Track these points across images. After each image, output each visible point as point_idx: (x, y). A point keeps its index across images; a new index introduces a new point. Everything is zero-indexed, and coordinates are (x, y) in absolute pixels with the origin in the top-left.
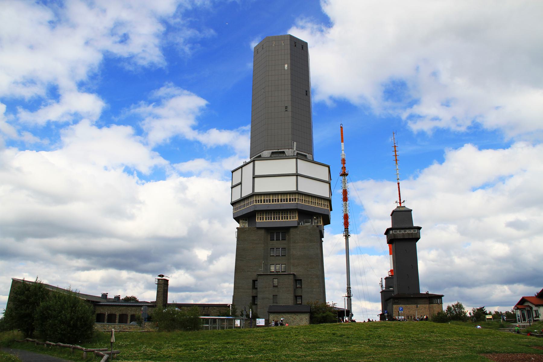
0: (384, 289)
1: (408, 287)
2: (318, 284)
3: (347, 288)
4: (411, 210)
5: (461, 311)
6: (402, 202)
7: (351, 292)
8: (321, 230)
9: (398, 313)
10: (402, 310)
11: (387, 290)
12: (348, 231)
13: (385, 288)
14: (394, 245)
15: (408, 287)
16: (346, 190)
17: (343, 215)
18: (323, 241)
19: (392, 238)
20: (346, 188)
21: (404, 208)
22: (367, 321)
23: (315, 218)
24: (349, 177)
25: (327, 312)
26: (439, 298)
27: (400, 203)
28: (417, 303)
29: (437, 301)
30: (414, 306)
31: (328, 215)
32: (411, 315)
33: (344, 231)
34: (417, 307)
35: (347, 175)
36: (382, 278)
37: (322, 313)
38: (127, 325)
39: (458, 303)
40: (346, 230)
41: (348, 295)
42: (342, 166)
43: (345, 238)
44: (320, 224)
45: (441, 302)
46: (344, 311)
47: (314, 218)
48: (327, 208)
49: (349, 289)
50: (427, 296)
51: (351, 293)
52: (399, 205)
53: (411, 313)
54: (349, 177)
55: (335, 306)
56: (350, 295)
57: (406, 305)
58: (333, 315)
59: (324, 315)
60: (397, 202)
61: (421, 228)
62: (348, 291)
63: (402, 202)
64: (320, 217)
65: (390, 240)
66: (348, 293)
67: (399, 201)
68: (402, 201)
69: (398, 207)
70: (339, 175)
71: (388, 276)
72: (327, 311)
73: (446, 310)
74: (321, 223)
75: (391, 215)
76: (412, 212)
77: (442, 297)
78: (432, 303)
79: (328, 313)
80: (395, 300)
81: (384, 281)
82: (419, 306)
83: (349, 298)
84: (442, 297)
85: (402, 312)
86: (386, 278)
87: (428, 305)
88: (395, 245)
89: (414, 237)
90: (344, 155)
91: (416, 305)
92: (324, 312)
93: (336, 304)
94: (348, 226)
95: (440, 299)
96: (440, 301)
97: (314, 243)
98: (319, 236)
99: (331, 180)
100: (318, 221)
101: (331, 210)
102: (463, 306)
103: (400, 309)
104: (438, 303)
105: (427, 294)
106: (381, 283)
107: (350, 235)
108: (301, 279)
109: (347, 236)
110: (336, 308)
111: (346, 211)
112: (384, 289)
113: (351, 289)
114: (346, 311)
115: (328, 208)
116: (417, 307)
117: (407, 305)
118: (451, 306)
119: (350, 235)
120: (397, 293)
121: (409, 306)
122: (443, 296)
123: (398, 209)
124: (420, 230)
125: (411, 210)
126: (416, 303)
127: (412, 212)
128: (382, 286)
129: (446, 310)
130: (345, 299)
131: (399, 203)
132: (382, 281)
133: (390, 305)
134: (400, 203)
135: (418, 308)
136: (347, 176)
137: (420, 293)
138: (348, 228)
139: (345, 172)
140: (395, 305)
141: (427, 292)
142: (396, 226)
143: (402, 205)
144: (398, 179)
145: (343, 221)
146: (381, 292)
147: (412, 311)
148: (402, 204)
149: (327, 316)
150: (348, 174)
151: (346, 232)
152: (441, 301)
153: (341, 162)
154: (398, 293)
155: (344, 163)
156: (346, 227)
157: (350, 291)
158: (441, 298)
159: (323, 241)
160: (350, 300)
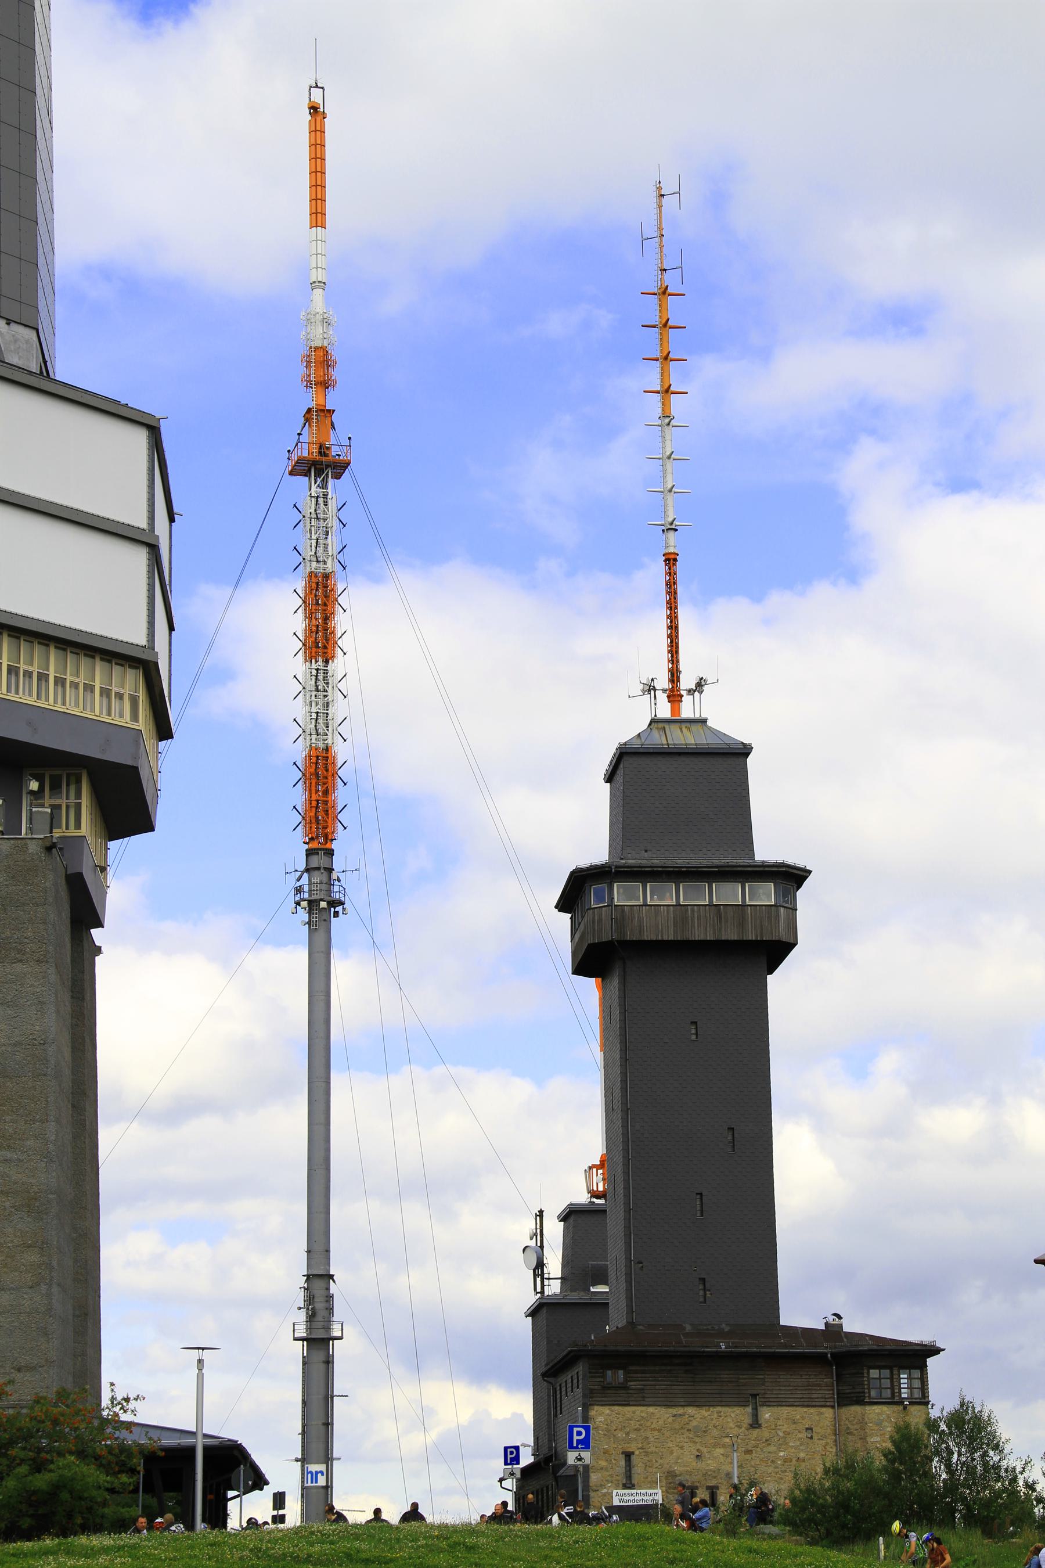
0: (554, 1288)
1: (703, 1280)
2: (33, 1257)
3: (308, 1277)
4: (745, 751)
5: (985, 1464)
6: (690, 692)
7: (330, 1310)
8: (80, 875)
9: (623, 1463)
10: (585, 1443)
11: (574, 1297)
12: (330, 870)
13: (563, 1279)
14: (615, 982)
15: (703, 1280)
16: (327, 576)
17: (299, 752)
18: (98, 950)
19: (606, 937)
20: (330, 567)
21: (695, 728)
22: (392, 1515)
23: (34, 785)
24: (355, 481)
25: (61, 1462)
26: (909, 1367)
27: (674, 697)
28: (754, 1396)
29: (895, 1387)
30: (735, 1416)
31: (135, 770)
32: (712, 1483)
33: (302, 866)
34: (755, 1424)
35: (340, 468)
36: (541, 1214)
37: (23, 1469)
38: (60, 857)
39: (962, 1405)
40: (315, 861)
41: (309, 1329)
42: (309, 399)
43: (306, 917)
44: (72, 832)
45: (917, 1394)
46: (191, 1450)
47: (28, 786)
48: (126, 721)
49: (318, 1284)
50: (826, 1348)
51: (337, 1316)
52: (664, 710)
53: (710, 1464)
54: (355, 481)
55: (125, 1417)
56: (328, 1328)
57: (680, 1411)
58: (103, 1478)
59: (41, 1481)
60: (650, 689)
61: (810, 872)
62: (310, 1299)
63: (690, 692)
64: (78, 782)
65: (591, 947)
66: (311, 1317)
67: (663, 682)
68: (687, 682)
69: (655, 722)
70: (284, 465)
71: (582, 1198)
72: (60, 1454)
73: (886, 1454)
74: (78, 826)
75: (610, 778)
76: (749, 760)
77: (930, 1361)
78: (860, 1401)
79: (69, 1466)
80: (609, 1373)
81: (555, 1231)
82: (766, 1414)
83: (319, 1356)
84: (930, 1361)
85: (586, 1455)
86: (571, 1215)
87: (828, 1413)
88: (623, 983)
89: (751, 936)
90: (326, 322)
91: (749, 1409)
92: (38, 1467)
93: (132, 1405)
94: (328, 838)
95: (916, 1373)
96: (910, 1388)
97: (19, 967)
98: (59, 916)
99: (172, 519)
100: (56, 808)
101: (164, 731)
102: (999, 1432)
103: (575, 1438)
104: (900, 1402)
105: (833, 1331)
106: (532, 1243)
107: (341, 903)
108: (696, 1021)
109: (323, 904)
110: (129, 1426)
111: (321, 728)
112: (554, 1288)
113: (333, 1288)
114: (207, 1449)
115: (135, 717)
116: (755, 1424)
117: (690, 1410)
118: (921, 1427)
119: (341, 903)
120: (622, 1323)
121: (704, 1412)
122: (934, 1351)
123: (658, 739)
124: (799, 886)
125: (745, 751)
126: (754, 1400)
127: (752, 762)
128: (540, 1265)
129: (886, 1454)
130: (200, 1361)
131: (662, 698)
132: (539, 1234)
133: (572, 1402)
134: (674, 697)
135: (765, 1433)
136: (338, 476)
137: (783, 1322)
138: (330, 853)
139: (323, 450)
140: (606, 1410)
141: (831, 1319)
142: (633, 860)
143: (687, 710)
144: (671, 528)
145: (298, 797)
146: (534, 1313)
147: (720, 1451)
148: (687, 700)
149: (57, 1488)
150: (345, 465)
151: (317, 878)
152: (917, 1384)
153: (302, 370)
154: (631, 1324)
155: (325, 384)
156: (314, 845)
157: (329, 1298)
158: (923, 1367)
159: (98, 950)
160: (322, 1366)
